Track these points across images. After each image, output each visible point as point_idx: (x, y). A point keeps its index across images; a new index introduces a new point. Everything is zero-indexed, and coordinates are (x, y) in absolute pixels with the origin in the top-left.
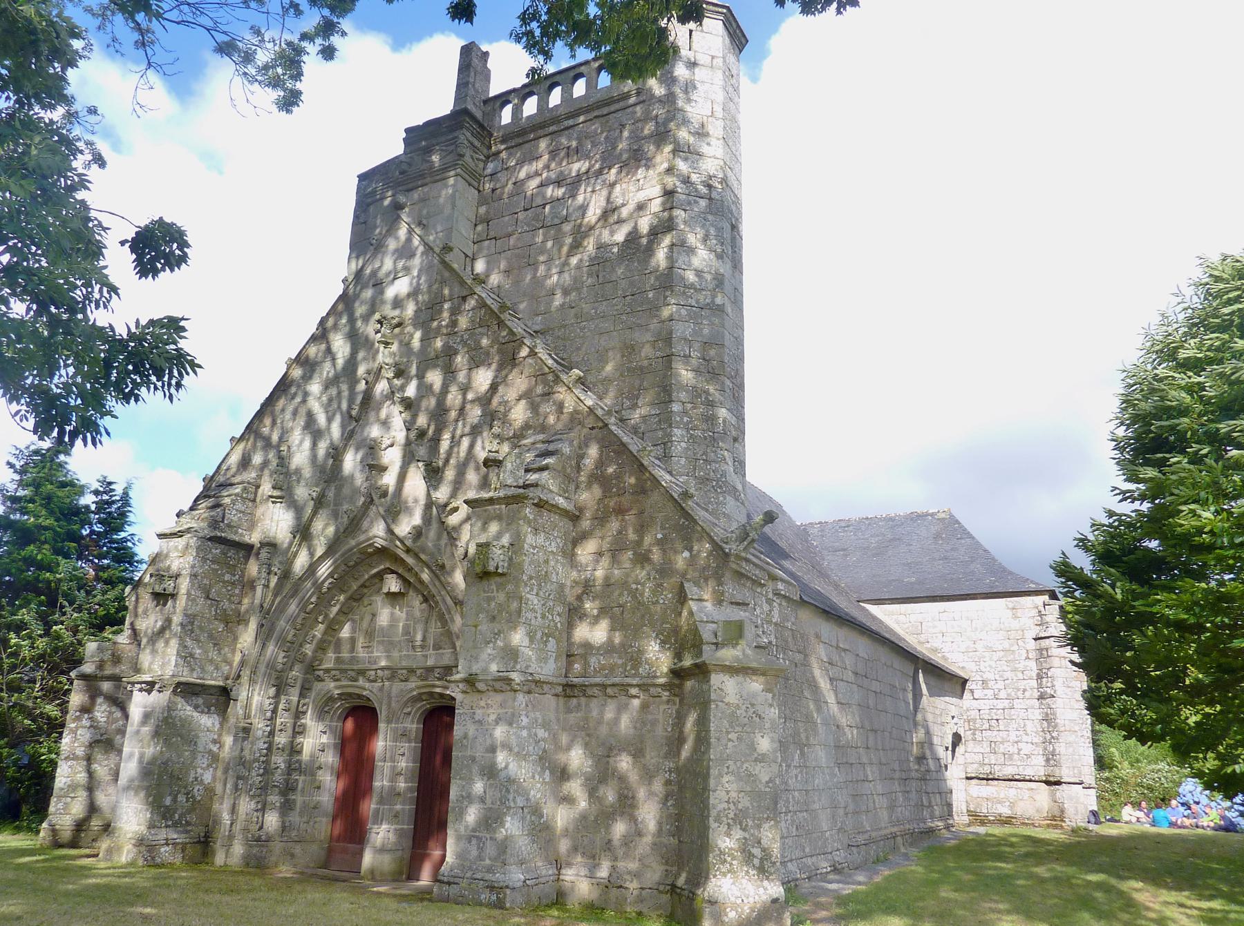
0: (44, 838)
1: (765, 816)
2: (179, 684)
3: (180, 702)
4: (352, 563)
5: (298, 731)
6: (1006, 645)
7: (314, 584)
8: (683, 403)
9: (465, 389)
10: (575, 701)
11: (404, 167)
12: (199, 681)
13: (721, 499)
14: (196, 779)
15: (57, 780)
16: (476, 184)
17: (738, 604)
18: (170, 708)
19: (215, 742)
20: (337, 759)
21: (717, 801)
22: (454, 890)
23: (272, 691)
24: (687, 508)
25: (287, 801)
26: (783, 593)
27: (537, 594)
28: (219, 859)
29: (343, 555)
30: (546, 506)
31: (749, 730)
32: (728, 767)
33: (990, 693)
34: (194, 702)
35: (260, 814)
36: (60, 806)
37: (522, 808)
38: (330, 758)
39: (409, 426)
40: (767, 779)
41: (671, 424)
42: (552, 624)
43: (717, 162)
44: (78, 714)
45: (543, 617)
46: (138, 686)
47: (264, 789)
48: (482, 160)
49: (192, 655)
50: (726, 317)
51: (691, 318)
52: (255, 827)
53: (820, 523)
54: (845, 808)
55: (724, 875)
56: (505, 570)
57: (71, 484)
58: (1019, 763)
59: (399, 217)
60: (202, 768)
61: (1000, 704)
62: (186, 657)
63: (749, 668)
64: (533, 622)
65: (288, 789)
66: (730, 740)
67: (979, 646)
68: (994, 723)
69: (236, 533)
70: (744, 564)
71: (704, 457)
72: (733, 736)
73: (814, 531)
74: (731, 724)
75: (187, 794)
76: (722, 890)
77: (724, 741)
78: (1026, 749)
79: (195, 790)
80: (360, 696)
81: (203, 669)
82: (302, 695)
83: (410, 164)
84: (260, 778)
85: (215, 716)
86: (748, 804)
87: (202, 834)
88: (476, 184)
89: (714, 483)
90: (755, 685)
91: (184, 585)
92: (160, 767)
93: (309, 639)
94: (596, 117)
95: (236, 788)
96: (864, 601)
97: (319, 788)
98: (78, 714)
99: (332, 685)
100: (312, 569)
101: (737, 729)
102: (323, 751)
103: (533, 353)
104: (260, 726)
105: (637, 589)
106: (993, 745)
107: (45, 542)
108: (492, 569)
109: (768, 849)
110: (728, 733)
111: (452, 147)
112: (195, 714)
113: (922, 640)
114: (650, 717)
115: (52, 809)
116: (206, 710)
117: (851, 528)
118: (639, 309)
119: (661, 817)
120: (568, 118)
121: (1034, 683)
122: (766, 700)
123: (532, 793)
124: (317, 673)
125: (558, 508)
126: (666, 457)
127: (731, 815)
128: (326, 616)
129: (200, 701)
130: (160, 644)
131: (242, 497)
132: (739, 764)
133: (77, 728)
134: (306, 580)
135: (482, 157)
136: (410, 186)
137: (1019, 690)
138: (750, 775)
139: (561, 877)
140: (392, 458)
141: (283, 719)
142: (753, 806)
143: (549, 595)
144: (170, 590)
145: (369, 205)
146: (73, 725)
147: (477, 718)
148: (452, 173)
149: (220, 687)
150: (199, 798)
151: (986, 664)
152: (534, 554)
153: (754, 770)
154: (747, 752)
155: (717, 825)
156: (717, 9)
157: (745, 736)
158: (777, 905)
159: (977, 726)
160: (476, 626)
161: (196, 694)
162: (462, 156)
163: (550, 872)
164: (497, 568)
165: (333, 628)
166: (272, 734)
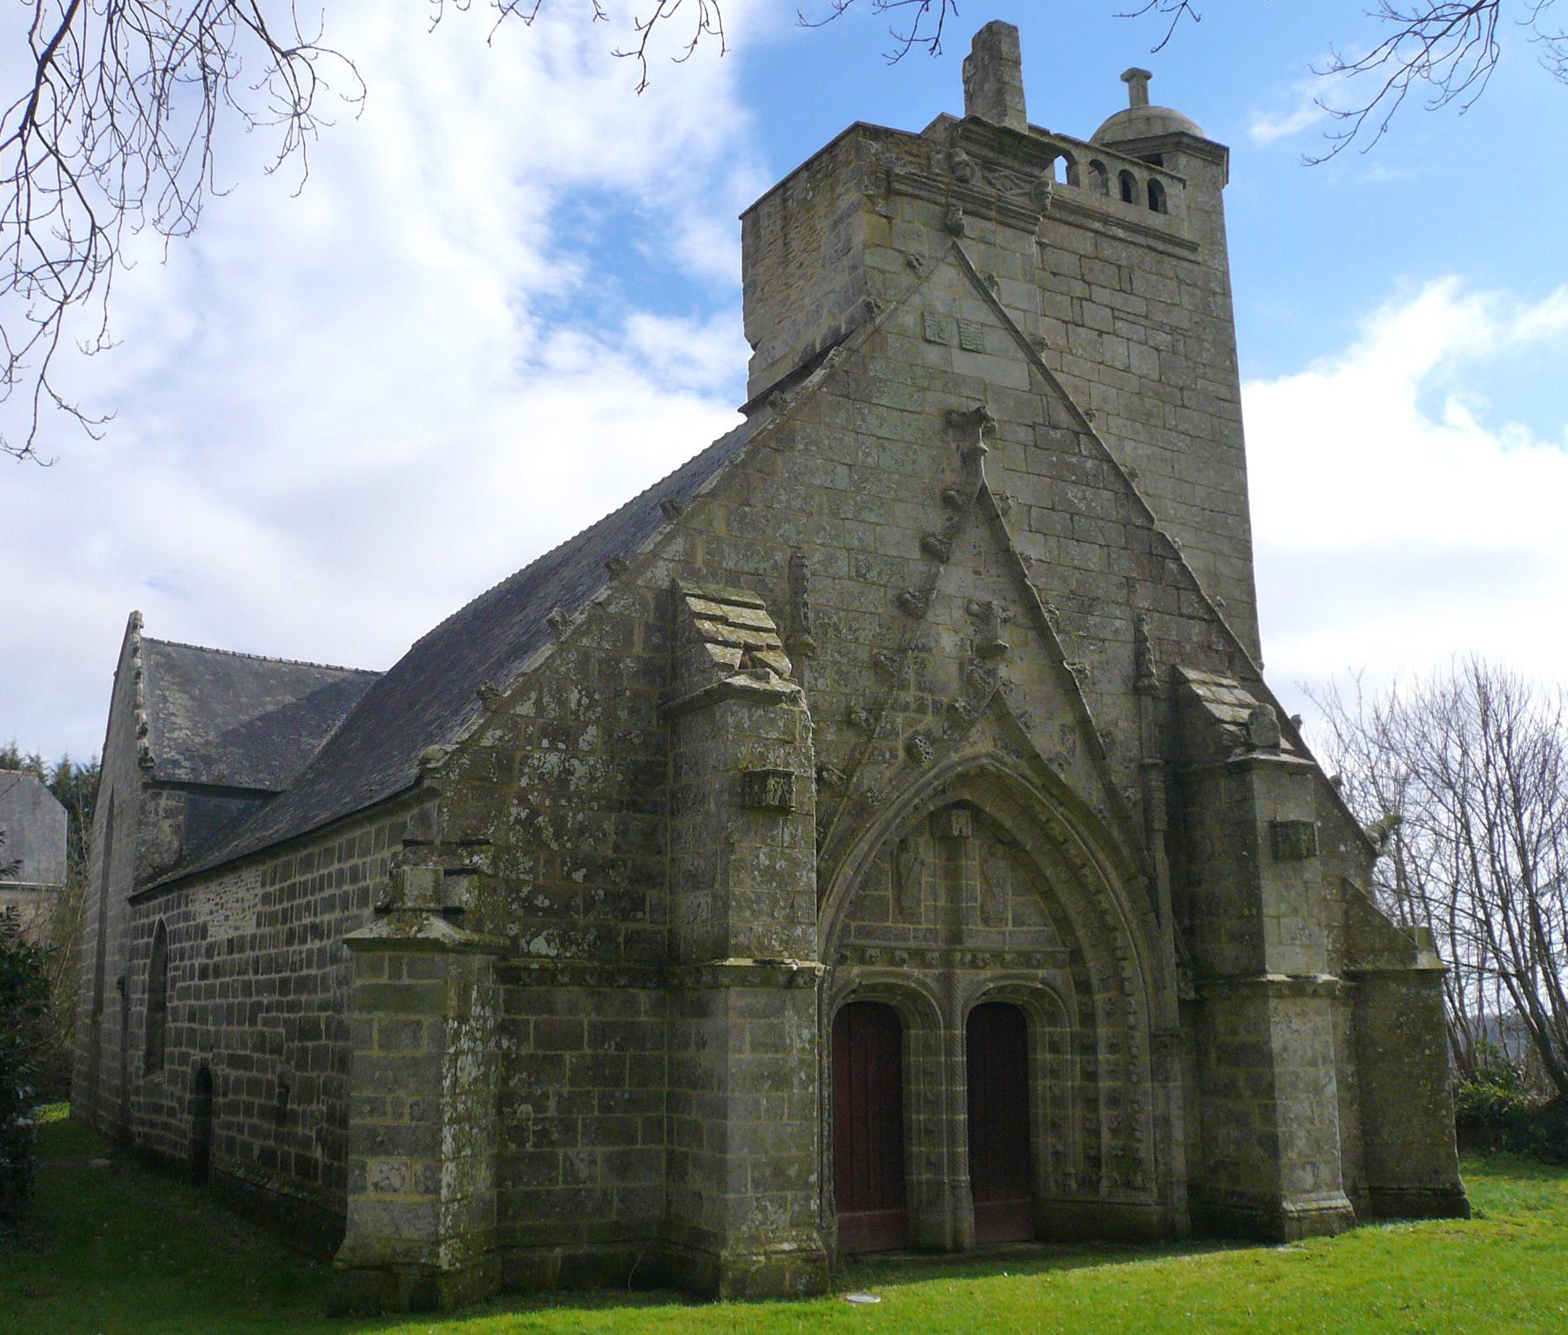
94: (1149, 247)
147: (1294, 1027)
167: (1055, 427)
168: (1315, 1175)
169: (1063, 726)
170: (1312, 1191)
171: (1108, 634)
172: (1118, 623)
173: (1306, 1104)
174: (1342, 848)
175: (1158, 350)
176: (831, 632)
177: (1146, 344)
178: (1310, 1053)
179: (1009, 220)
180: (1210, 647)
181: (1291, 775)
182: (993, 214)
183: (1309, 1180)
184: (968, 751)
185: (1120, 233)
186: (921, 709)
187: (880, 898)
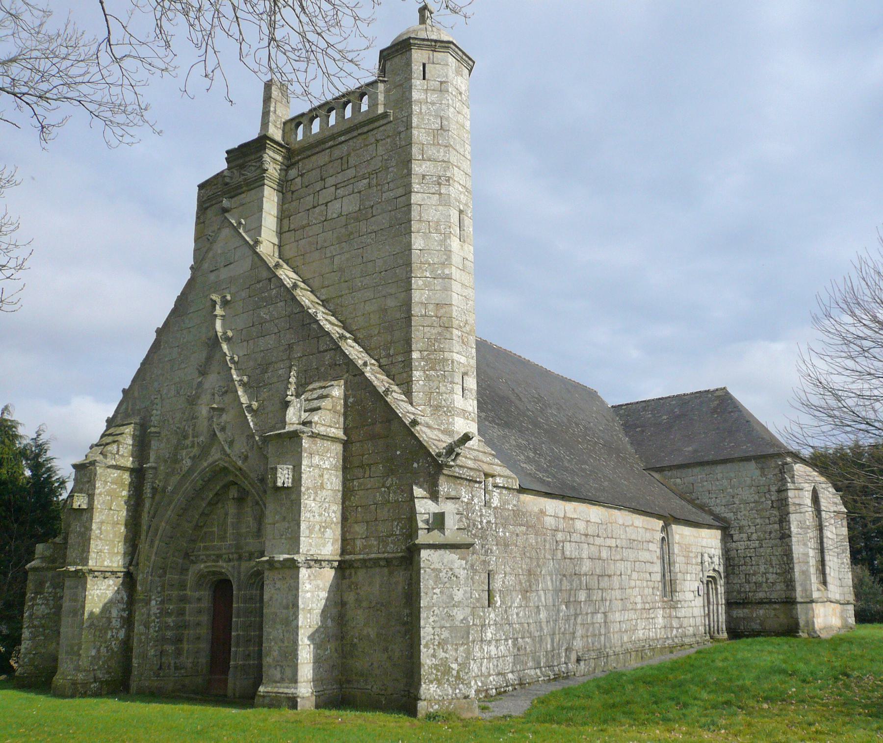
1: (461, 642)
6: (756, 497)
8: (421, 351)
11: (227, 180)
13: (451, 420)
25: (177, 649)
27: (314, 500)
29: (199, 474)
31: (448, 586)
33: (744, 536)
40: (462, 617)
41: (411, 368)
42: (328, 519)
45: (320, 515)
56: (290, 485)
58: (767, 590)
61: (754, 544)
64: (312, 519)
66: (435, 593)
67: (737, 501)
68: (748, 560)
71: (437, 390)
72: (437, 591)
74: (435, 583)
77: (431, 595)
78: (772, 578)
80: (221, 573)
83: (231, 178)
86: (448, 635)
89: (445, 409)
94: (359, 134)
101: (440, 586)
105: (385, 491)
106: (747, 577)
108: (279, 484)
110: (433, 589)
111: (258, 164)
114: (395, 580)
118: (390, 281)
121: (777, 526)
124: (191, 558)
125: (329, 437)
126: (408, 393)
127: (436, 643)
132: (441, 609)
136: (232, 194)
137: (766, 532)
138: (450, 616)
142: (452, 637)
143: (325, 499)
145: (206, 208)
147: (277, 586)
151: (742, 514)
152: (310, 472)
153: (453, 612)
159: (736, 562)
164: (284, 483)
167: (259, 282)
168: (282, 673)
169: (248, 436)
170: (279, 682)
171: (275, 380)
172: (280, 372)
173: (280, 631)
174: (415, 465)
175: (360, 192)
176: (166, 422)
177: (353, 193)
178: (285, 601)
179: (252, 186)
180: (336, 365)
181: (290, 438)
182: (245, 188)
183: (278, 676)
184: (210, 460)
185: (343, 138)
186: (193, 446)
187: (212, 532)
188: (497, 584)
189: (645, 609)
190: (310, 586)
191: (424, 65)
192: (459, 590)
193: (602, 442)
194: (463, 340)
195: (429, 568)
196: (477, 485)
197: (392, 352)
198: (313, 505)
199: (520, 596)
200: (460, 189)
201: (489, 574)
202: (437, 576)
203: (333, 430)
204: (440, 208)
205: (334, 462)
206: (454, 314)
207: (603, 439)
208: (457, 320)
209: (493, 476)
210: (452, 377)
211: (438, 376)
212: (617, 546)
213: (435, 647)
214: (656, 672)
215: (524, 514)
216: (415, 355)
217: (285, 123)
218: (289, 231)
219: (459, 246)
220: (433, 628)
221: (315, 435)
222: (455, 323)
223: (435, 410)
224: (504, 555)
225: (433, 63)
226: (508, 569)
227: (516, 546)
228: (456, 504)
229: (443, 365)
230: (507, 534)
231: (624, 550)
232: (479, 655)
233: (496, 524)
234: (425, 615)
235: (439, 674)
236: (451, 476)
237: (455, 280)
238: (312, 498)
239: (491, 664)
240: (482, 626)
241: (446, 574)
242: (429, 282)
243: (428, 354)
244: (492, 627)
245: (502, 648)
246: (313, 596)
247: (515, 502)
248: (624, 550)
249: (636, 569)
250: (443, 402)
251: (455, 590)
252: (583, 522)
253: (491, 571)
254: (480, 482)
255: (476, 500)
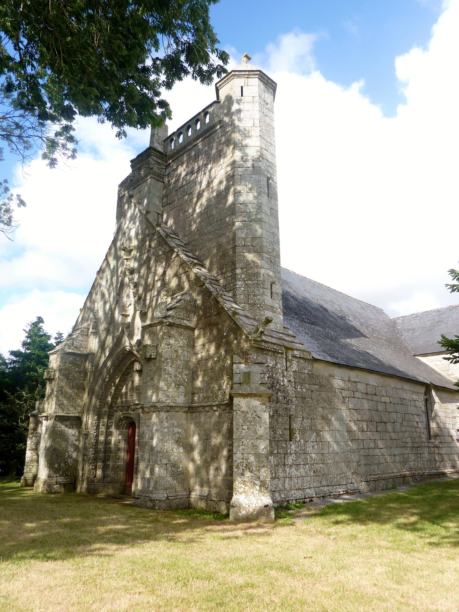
0: (22, 483)
1: (262, 465)
2: (56, 416)
3: (59, 424)
4: (120, 359)
5: (108, 434)
7: (107, 369)
8: (242, 269)
9: (155, 274)
10: (195, 414)
11: (132, 178)
12: (67, 415)
13: (262, 313)
14: (69, 456)
15: (26, 459)
16: (162, 180)
17: (259, 363)
18: (54, 427)
19: (76, 440)
20: (126, 446)
21: (237, 458)
22: (139, 501)
23: (96, 417)
24: (235, 319)
26: (298, 356)
28: (78, 490)
29: (116, 355)
30: (174, 325)
32: (242, 442)
34: (65, 424)
35: (94, 471)
36: (28, 469)
37: (166, 464)
38: (123, 445)
39: (135, 294)
41: (236, 280)
43: (256, 148)
44: (32, 431)
45: (176, 376)
46: (44, 418)
47: (95, 460)
48: (164, 169)
49: (62, 404)
50: (263, 223)
51: (245, 227)
52: (92, 476)
53: (403, 317)
54: (358, 462)
55: (241, 493)
57: (45, 335)
59: (131, 202)
60: (71, 452)
62: (60, 405)
63: (252, 394)
65: (105, 460)
66: (243, 429)
69: (80, 350)
70: (263, 344)
71: (253, 294)
72: (245, 427)
73: (399, 321)
75: (65, 463)
76: (239, 501)
77: (240, 430)
79: (69, 461)
80: (131, 418)
81: (68, 409)
82: (108, 419)
83: (134, 177)
84: (93, 455)
85: (76, 429)
87: (73, 480)
88: (162, 180)
89: (259, 305)
90: (256, 403)
91: (57, 375)
92: (51, 452)
93: (109, 393)
95: (84, 460)
96: (417, 356)
97: (119, 459)
98: (32, 431)
99: (121, 413)
100: (105, 363)
101: (247, 424)
102: (120, 443)
103: (178, 255)
104: (93, 432)
107: (33, 359)
109: (264, 481)
110: (242, 426)
112: (66, 429)
113: (450, 373)
114: (222, 420)
115: (25, 471)
116: (71, 427)
117: (418, 318)
119: (227, 467)
120: (194, 141)
122: (262, 409)
123: (172, 457)
124: (114, 408)
125: (182, 326)
128: (115, 383)
129: (68, 423)
130: (50, 400)
131: (81, 334)
132: (248, 440)
133: (32, 437)
134: (103, 368)
135: (164, 167)
139: (191, 496)
140: (130, 311)
141: (102, 429)
143: (179, 366)
144: (52, 377)
146: (31, 436)
148: (149, 177)
149: (77, 417)
150: (71, 465)
153: (256, 443)
154: (253, 434)
155: (237, 470)
156: (254, 73)
157: (251, 427)
158: (267, 508)
160: (146, 383)
161: (66, 420)
162: (152, 168)
163: (184, 494)
165: (118, 388)
166: (97, 436)
188: (295, 426)
189: (414, 447)
190: (167, 424)
191: (242, 87)
192: (261, 427)
193: (384, 338)
194: (271, 261)
195: (239, 411)
196: (280, 355)
197: (224, 271)
198: (170, 370)
199: (315, 434)
200: (268, 164)
201: (290, 418)
202: (245, 416)
203: (185, 321)
204: (253, 176)
205: (186, 343)
206: (265, 244)
207: (385, 337)
208: (267, 247)
209: (292, 349)
210: (263, 284)
211: (253, 284)
212: (390, 402)
213: (244, 468)
214: (40, 534)
215: (317, 377)
216: (238, 271)
217: (164, 141)
218: (167, 205)
219: (267, 201)
220: (242, 454)
221: (172, 324)
222: (265, 249)
223: (251, 306)
224: (302, 405)
225: (248, 85)
226: (305, 415)
227: (312, 399)
228: (262, 367)
229: (257, 277)
230: (304, 390)
231: (396, 405)
232: (281, 475)
233: (295, 382)
234: (237, 445)
235: (246, 488)
236: (259, 348)
237: (265, 222)
238: (169, 365)
239: (292, 482)
240: (285, 454)
241: (252, 415)
242: (247, 224)
243: (247, 270)
244: (293, 455)
245: (302, 470)
246: (169, 431)
247: (310, 369)
248: (396, 405)
249: (406, 419)
250: (257, 301)
251: (258, 427)
252: (363, 385)
253: (292, 415)
254: (282, 354)
255: (279, 366)
